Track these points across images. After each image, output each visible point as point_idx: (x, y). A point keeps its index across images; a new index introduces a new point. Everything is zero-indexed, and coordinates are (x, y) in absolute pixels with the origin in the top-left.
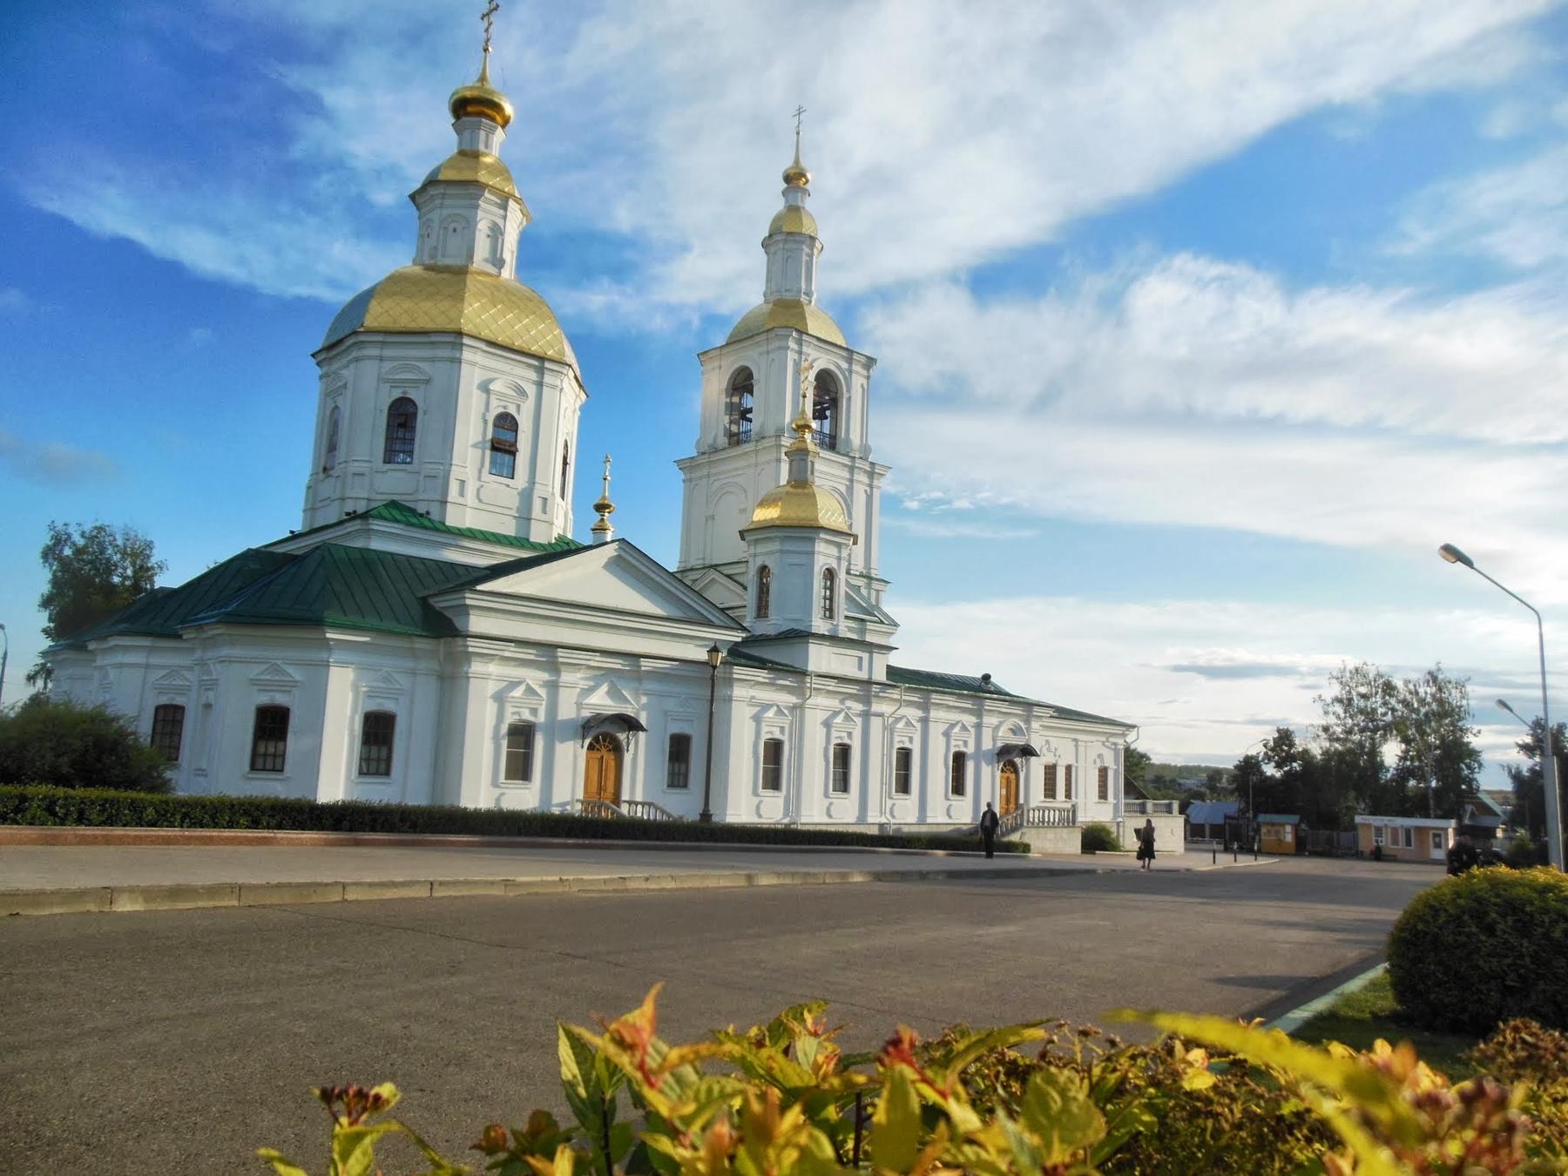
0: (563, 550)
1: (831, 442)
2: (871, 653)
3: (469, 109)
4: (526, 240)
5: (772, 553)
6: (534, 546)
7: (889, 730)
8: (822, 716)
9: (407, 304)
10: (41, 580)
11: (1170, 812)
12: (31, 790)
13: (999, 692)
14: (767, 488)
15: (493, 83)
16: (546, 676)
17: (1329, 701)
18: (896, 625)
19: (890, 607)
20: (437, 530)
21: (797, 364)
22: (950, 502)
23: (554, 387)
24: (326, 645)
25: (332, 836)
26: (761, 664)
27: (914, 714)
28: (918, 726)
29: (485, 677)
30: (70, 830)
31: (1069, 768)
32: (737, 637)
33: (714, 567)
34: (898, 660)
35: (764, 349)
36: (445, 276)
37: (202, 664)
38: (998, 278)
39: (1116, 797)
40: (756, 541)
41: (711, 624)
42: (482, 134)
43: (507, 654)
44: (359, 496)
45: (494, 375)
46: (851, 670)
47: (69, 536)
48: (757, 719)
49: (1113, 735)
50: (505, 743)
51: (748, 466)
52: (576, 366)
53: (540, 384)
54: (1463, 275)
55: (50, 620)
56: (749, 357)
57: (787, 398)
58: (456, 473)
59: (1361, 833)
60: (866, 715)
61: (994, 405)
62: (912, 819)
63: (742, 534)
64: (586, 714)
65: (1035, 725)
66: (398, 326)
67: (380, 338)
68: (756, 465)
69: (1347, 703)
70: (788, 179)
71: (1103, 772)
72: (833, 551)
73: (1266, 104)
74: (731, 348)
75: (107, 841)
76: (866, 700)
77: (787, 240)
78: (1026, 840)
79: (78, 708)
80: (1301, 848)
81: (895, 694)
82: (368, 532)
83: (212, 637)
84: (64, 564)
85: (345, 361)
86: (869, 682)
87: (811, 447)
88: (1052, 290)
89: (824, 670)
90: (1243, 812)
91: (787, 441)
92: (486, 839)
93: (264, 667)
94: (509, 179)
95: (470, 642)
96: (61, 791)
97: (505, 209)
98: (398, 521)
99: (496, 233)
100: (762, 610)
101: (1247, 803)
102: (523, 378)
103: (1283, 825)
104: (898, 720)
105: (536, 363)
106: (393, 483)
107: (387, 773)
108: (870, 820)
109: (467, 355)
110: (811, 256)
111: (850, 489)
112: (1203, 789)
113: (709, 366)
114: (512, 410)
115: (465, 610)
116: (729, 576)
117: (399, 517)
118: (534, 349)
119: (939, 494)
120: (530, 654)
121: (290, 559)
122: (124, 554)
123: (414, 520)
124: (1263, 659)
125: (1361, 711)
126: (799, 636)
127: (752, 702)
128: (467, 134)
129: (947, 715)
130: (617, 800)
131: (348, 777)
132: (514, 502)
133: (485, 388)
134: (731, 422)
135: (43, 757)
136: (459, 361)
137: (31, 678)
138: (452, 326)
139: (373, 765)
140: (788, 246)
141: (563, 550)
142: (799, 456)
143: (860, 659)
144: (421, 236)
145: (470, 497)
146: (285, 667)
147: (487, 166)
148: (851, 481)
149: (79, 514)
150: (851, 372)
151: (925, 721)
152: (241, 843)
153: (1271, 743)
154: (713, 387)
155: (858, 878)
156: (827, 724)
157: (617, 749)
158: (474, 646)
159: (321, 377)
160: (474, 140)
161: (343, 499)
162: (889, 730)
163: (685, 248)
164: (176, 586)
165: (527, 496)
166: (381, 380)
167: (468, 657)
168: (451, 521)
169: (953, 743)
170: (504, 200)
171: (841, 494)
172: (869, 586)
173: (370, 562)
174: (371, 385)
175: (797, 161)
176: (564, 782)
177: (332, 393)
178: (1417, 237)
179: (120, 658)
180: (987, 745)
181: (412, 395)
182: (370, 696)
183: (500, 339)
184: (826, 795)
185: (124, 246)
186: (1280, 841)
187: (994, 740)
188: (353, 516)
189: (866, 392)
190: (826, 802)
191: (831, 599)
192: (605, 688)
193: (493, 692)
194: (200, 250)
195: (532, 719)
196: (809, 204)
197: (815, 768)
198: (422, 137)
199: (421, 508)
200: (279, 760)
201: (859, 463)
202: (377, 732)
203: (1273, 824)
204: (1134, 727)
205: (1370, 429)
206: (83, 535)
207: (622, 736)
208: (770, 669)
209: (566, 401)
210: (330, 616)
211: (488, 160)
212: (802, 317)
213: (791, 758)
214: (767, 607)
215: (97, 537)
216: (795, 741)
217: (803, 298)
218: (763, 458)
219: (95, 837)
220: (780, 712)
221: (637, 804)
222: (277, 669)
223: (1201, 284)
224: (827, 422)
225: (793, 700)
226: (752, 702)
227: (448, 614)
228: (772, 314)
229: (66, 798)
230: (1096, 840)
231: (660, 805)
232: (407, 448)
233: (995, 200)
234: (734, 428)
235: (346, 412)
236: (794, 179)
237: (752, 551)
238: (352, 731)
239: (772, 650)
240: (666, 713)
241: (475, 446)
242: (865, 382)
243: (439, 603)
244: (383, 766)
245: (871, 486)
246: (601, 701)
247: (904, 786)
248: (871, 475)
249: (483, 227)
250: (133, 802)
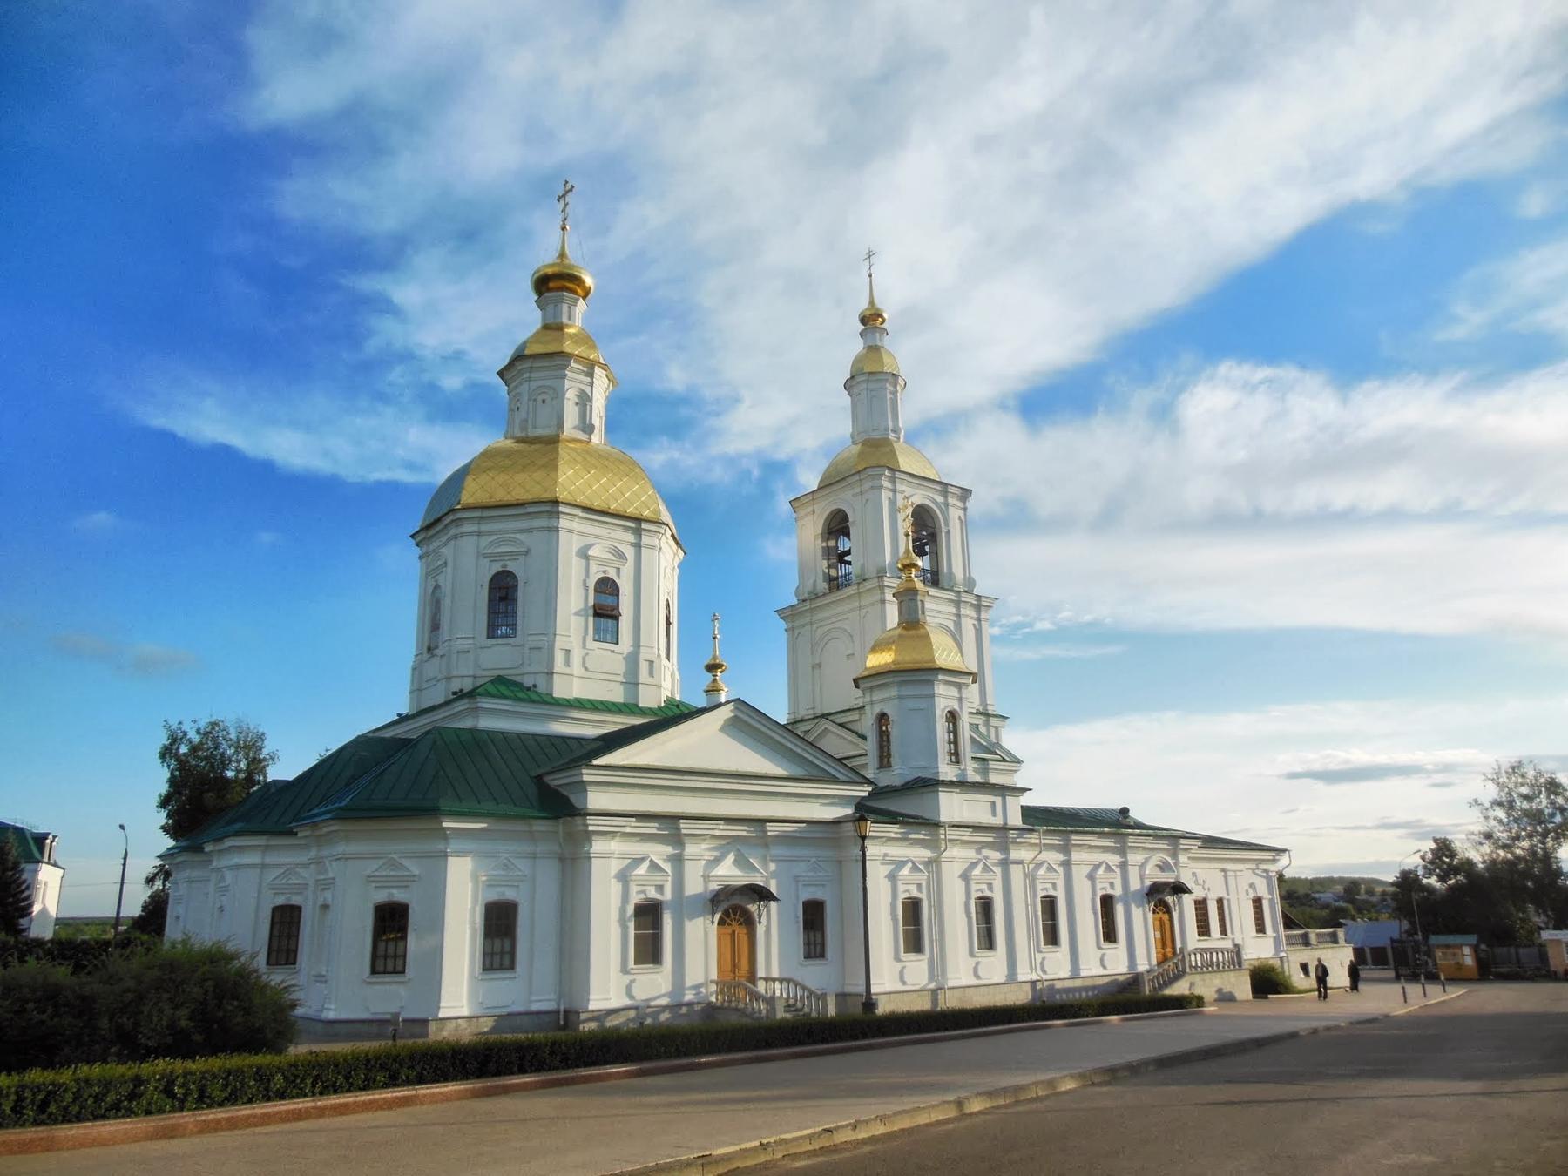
0: (673, 716)
1: (934, 578)
2: (1004, 797)
3: (551, 285)
4: (615, 405)
5: (890, 699)
6: (644, 712)
7: (1031, 877)
8: (959, 868)
9: (502, 478)
10: (159, 779)
11: (1336, 942)
12: (146, 1069)
13: (1139, 826)
14: (875, 635)
15: (574, 257)
16: (669, 850)
17: (1487, 805)
18: (1019, 762)
19: (1011, 740)
20: (545, 703)
21: (893, 502)
22: (1031, 625)
23: (653, 547)
24: (443, 834)
25: (478, 1084)
26: (891, 818)
27: (1054, 857)
28: (1060, 870)
29: (606, 856)
30: (187, 1118)
31: (1220, 901)
32: (863, 791)
33: (825, 716)
34: (1028, 800)
36: (537, 446)
37: (318, 862)
38: (1047, 401)
39: (1275, 929)
40: (872, 688)
41: (835, 781)
42: (565, 307)
43: (628, 830)
44: (464, 675)
45: (592, 541)
46: (986, 819)
47: (185, 734)
48: (892, 877)
49: (1263, 861)
50: (632, 925)
51: (852, 610)
52: (671, 524)
53: (638, 546)
54: (1518, 354)
55: (169, 817)
56: (844, 499)
57: (886, 539)
58: (560, 642)
59: (1551, 952)
60: (1005, 864)
61: (1059, 524)
62: (1065, 972)
63: (857, 682)
64: (714, 886)
65: (1183, 859)
66: (493, 502)
67: (477, 514)
68: (811, 624)
69: (1509, 806)
70: (864, 320)
71: (1257, 902)
72: (954, 692)
73: (1289, 211)
74: (828, 490)
75: (232, 1124)
76: (1004, 847)
77: (870, 380)
78: (1197, 992)
79: (197, 947)
80: (1486, 971)
81: (1033, 838)
82: (476, 711)
83: (328, 834)
84: (182, 763)
85: (444, 539)
86: (1004, 829)
87: (919, 585)
88: (1101, 409)
89: (956, 819)
90: (1410, 933)
91: (891, 583)
92: (646, 1065)
93: (381, 862)
94: (593, 347)
95: (591, 820)
96: (179, 1066)
97: (592, 376)
98: (505, 697)
99: (584, 400)
100: (884, 761)
101: (1412, 923)
102: (621, 541)
103: (1460, 946)
104: (1039, 866)
105: (632, 525)
106: (498, 658)
107: (512, 967)
108: (1021, 978)
109: (564, 523)
110: (895, 393)
111: (958, 624)
112: (1341, 904)
113: (802, 513)
114: (612, 574)
115: (582, 786)
116: (841, 725)
117: (506, 692)
118: (630, 511)
119: (1020, 618)
120: (651, 828)
121: (404, 744)
122: (238, 747)
123: (521, 695)
124: (1382, 759)
125: (1526, 813)
126: (927, 785)
127: (886, 860)
128: (550, 308)
129: (1089, 854)
130: (752, 978)
131: (472, 976)
132: (620, 667)
133: (584, 554)
134: (829, 567)
135: (161, 1011)
136: (557, 530)
137: (150, 881)
138: (547, 496)
139: (497, 959)
140: (871, 386)
141: (673, 716)
142: (907, 597)
143: (993, 804)
144: (511, 410)
145: (576, 668)
146: (403, 861)
147: (571, 336)
148: (958, 615)
149: (192, 718)
150: (947, 505)
151: (1067, 865)
152: (380, 1108)
153: (1430, 855)
154: (811, 529)
155: (1070, 1085)
156: (965, 877)
157: (749, 922)
158: (594, 824)
159: (421, 557)
160: (557, 314)
161: (449, 678)
162: (1031, 877)
163: (737, 400)
164: (291, 778)
165: (633, 660)
166: (482, 555)
167: (588, 836)
168: (560, 690)
169: (1099, 886)
170: (590, 368)
171: (950, 631)
172: (987, 723)
173: (479, 742)
174: (470, 561)
175: (872, 302)
176: (696, 963)
177: (432, 573)
178: (1468, 321)
179: (236, 859)
180: (1135, 885)
181: (511, 567)
182: (490, 885)
183: (596, 505)
184: (972, 954)
185: (225, 454)
186: (1459, 966)
187: (1142, 878)
188: (460, 695)
189: (964, 523)
190: (973, 961)
191: (956, 743)
192: (731, 857)
193: (616, 871)
194: (288, 446)
195: (659, 897)
196: (886, 342)
197: (957, 924)
198: (503, 317)
199: (528, 682)
200: (400, 962)
201: (964, 597)
202: (500, 923)
203: (1448, 946)
204: (1284, 851)
205: (1449, 513)
206: (198, 732)
207: (753, 908)
208: (902, 824)
209: (665, 560)
210: (444, 805)
211: (571, 331)
212: (893, 454)
213: (945, 927)
214: (889, 756)
215: (211, 732)
216: (934, 897)
217: (892, 436)
218: (866, 600)
219: (218, 1121)
220: (915, 868)
221: (774, 980)
222: (394, 865)
223: (1250, 388)
224: (927, 558)
225: (927, 854)
226: (886, 860)
228: (861, 454)
229: (185, 1075)
230: (1266, 982)
231: (799, 979)
232: (510, 621)
233: (1028, 325)
234: (833, 573)
235: (446, 588)
236: (871, 320)
237: (868, 699)
238: (473, 923)
239: (899, 802)
240: (796, 879)
241: (577, 614)
242: (961, 513)
243: (555, 781)
244: (507, 962)
245: (979, 619)
246: (729, 872)
247: (1052, 937)
248: (978, 608)
249: (571, 395)
250: (259, 1069)
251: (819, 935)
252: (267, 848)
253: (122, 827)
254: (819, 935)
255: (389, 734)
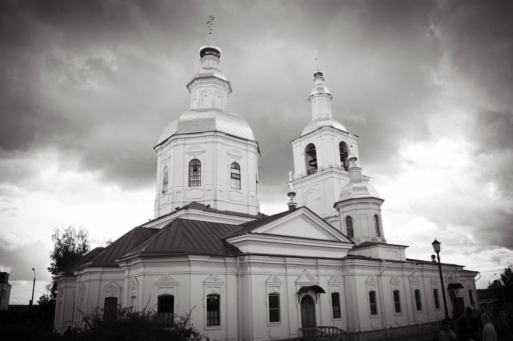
6: (252, 217)
35: (319, 135)
67: (184, 136)
68: (302, 187)
85: (169, 148)
140: (320, 98)
225: (377, 272)
227: (236, 246)
243: (231, 241)
251: (216, 313)
252: (102, 272)
253: (33, 269)
254: (216, 313)
255: (148, 226)
